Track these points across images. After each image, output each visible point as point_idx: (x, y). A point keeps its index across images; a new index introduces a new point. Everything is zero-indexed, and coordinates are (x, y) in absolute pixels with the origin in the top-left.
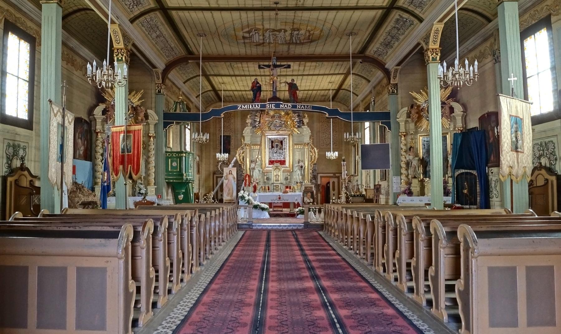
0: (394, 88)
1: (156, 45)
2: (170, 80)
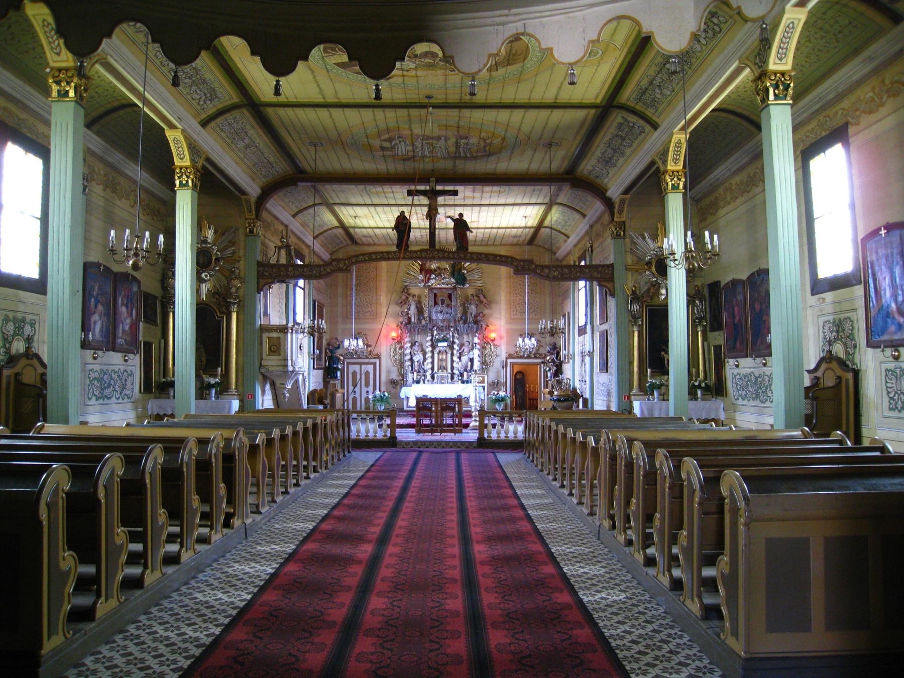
0: (620, 229)
1: (245, 160)
2: (269, 212)
